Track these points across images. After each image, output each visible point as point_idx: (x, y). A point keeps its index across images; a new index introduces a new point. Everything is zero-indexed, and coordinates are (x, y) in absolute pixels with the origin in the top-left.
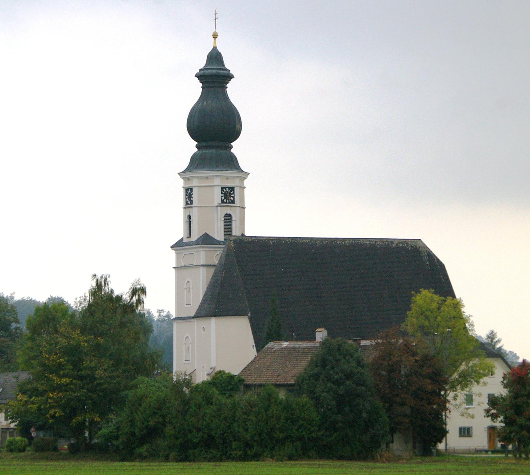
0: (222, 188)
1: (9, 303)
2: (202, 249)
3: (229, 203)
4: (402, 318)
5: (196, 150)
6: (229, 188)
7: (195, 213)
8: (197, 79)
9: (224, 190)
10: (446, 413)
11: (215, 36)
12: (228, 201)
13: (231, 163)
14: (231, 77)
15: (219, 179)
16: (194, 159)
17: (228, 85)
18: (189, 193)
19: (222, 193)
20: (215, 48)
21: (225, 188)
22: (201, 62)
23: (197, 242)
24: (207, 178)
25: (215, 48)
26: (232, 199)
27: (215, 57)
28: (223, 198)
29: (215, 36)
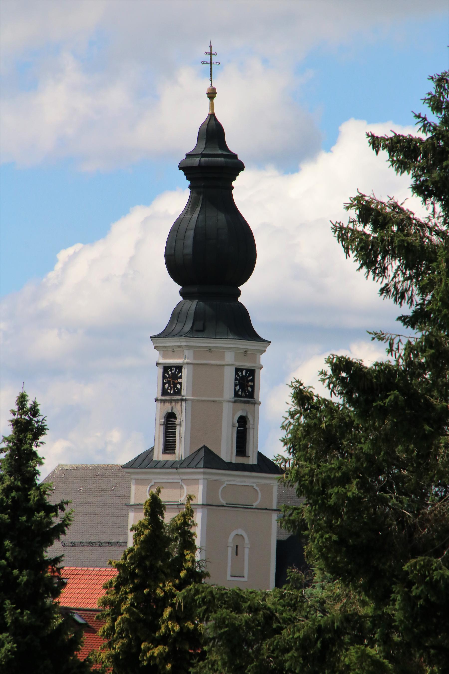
0: (238, 370)
1: (9, 649)
2: (202, 476)
3: (246, 396)
4: (292, 536)
5: (181, 299)
6: (247, 370)
7: (182, 412)
8: (182, 172)
9: (240, 373)
10: (36, 516)
11: (212, 94)
12: (244, 394)
13: (239, 324)
14: (240, 167)
15: (228, 352)
16: (177, 315)
17: (234, 184)
18: (171, 377)
19: (236, 379)
20: (212, 116)
21: (241, 370)
22: (189, 142)
23: (187, 463)
24: (210, 350)
25: (212, 116)
26: (250, 389)
27: (213, 132)
28: (238, 388)
29: (212, 94)
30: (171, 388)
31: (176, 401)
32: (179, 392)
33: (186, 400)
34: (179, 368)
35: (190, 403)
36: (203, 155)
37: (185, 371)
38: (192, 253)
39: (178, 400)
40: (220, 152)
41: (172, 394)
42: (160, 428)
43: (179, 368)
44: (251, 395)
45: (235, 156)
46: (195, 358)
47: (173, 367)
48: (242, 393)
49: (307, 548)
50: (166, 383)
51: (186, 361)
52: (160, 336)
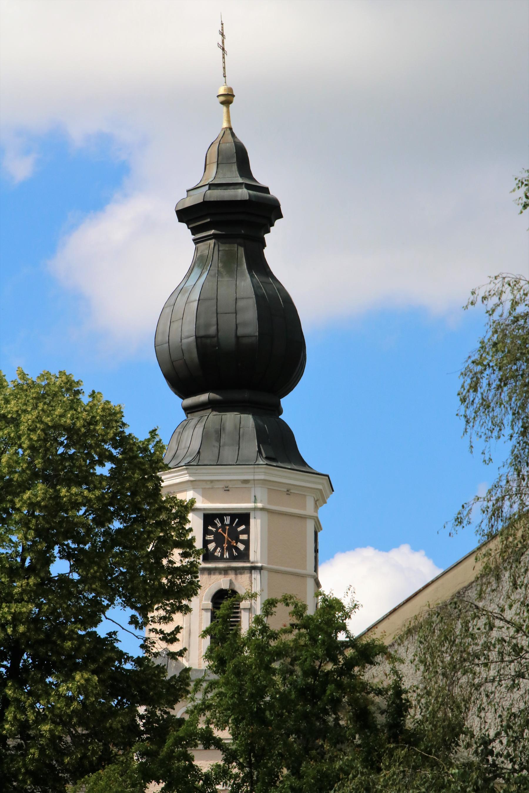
30: (222, 549)
31: (237, 571)
32: (244, 556)
33: (260, 569)
34: (244, 518)
35: (264, 572)
36: (212, 186)
37: (256, 525)
38: (257, 334)
39: (244, 568)
40: (240, 180)
41: (226, 559)
42: (201, 615)
43: (244, 518)
44: (234, 559)
45: (266, 190)
46: (269, 502)
47: (226, 515)
48: (222, 554)
49: (257, 787)
50: (210, 542)
51: (259, 505)
52: (180, 465)
